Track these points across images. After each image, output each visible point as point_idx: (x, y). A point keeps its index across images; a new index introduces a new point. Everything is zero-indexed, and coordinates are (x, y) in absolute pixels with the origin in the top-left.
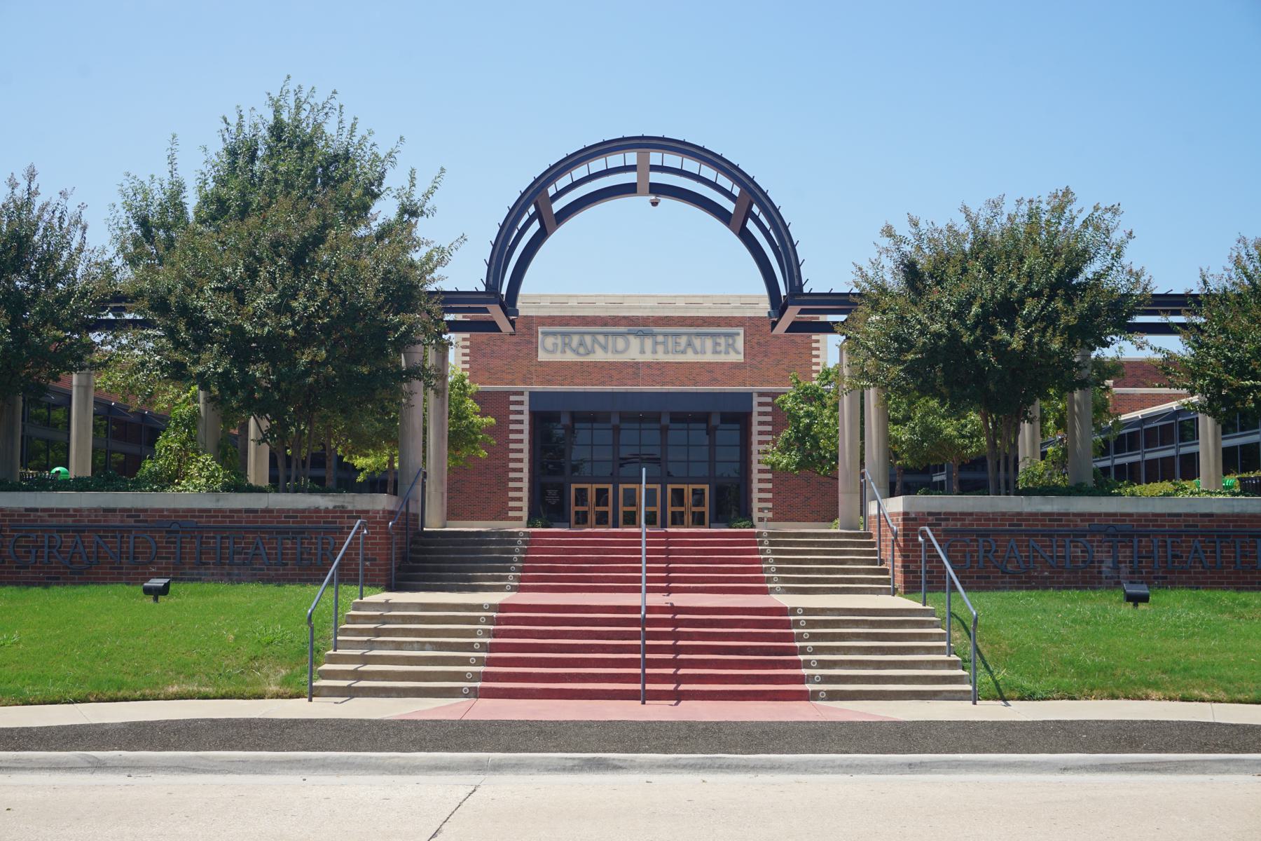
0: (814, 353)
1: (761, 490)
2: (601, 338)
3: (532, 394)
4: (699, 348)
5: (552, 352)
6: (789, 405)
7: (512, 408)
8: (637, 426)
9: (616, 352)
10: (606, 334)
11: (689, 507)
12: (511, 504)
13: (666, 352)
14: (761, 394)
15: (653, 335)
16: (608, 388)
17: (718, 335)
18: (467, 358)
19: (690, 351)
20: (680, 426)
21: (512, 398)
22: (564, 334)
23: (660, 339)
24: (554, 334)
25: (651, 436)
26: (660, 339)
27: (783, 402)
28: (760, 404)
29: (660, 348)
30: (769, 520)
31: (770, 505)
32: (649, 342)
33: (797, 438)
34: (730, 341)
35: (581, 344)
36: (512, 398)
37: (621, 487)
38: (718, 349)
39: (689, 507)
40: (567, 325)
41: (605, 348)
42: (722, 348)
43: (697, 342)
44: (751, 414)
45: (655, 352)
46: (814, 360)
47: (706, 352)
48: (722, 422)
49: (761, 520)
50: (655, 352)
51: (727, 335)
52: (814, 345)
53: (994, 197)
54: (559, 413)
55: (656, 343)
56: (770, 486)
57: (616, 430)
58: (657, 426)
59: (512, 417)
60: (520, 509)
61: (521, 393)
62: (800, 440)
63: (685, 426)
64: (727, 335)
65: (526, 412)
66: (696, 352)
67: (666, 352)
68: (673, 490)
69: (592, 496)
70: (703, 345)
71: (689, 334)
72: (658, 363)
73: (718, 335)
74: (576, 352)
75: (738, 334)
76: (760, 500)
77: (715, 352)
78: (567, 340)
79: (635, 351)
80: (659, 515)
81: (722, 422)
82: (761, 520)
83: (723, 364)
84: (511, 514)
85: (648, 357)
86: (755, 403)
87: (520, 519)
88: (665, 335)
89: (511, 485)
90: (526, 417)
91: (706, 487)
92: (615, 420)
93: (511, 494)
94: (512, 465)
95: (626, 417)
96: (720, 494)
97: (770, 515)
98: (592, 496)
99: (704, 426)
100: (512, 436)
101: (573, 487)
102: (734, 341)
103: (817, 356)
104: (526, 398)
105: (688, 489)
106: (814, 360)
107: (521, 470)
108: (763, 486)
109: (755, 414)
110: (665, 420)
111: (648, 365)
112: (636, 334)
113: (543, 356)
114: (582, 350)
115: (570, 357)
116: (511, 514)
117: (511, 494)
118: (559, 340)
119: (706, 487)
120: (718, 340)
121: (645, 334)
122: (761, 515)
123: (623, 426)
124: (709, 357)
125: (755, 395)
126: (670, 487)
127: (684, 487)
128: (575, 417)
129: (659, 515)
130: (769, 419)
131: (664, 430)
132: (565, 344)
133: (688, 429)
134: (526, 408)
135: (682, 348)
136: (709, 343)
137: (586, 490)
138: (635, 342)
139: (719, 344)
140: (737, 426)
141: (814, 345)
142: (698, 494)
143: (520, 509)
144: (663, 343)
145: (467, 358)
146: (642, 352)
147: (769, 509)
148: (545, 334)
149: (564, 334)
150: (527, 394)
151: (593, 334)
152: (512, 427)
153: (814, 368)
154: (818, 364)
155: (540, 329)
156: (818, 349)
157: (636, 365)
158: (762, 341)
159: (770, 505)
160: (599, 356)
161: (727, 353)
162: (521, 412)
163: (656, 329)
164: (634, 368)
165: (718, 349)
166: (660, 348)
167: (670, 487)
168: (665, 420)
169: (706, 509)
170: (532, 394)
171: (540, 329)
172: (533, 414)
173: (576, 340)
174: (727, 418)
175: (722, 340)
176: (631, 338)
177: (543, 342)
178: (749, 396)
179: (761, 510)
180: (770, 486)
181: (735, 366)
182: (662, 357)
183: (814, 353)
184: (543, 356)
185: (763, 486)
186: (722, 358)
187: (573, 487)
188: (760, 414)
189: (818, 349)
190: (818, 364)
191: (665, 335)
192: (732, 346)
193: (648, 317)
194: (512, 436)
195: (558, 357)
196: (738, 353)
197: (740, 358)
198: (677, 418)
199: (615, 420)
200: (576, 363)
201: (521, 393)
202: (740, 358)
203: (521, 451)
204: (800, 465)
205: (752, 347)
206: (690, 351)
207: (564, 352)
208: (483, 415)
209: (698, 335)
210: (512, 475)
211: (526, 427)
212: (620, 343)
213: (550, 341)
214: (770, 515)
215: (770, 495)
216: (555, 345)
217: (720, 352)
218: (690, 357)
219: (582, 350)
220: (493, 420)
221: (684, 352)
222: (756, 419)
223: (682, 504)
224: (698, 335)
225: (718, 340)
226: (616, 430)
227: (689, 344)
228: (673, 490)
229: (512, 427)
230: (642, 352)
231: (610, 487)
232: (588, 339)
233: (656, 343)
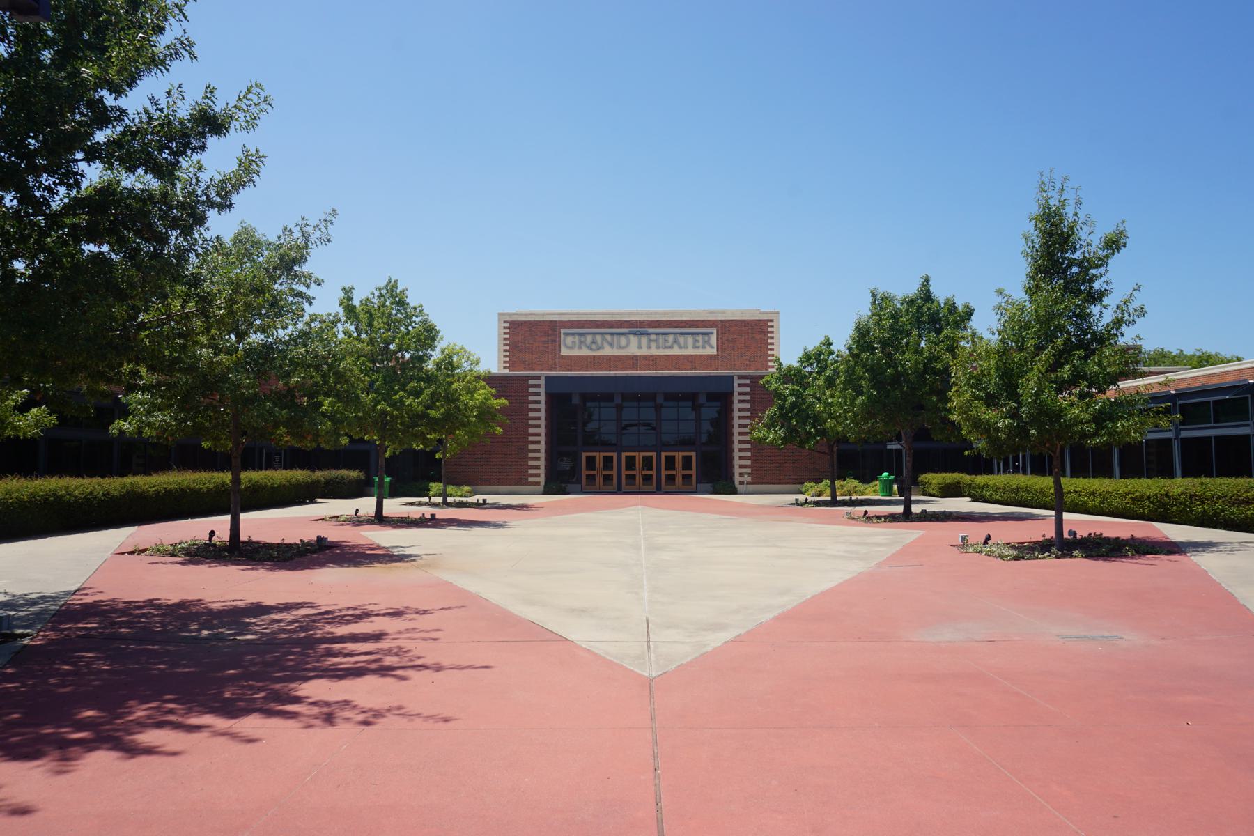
1: (741, 458)
2: (608, 338)
3: (548, 379)
6: (774, 385)
8: (636, 404)
9: (620, 347)
10: (612, 334)
11: (679, 471)
12: (531, 471)
13: (658, 347)
14: (741, 377)
15: (648, 334)
17: (698, 334)
19: (676, 346)
20: (671, 404)
21: (531, 382)
22: (581, 335)
23: (653, 337)
24: (573, 334)
25: (648, 414)
26: (653, 337)
27: (768, 382)
28: (740, 385)
29: (653, 345)
30: (749, 483)
31: (749, 471)
32: (644, 340)
33: (781, 414)
35: (594, 342)
36: (531, 382)
37: (624, 454)
39: (679, 471)
41: (611, 345)
43: (681, 339)
44: (732, 393)
45: (649, 347)
47: (688, 347)
48: (666, 399)
50: (649, 347)
51: (703, 334)
57: (619, 408)
61: (538, 378)
64: (703, 334)
65: (543, 393)
66: (680, 347)
67: (658, 347)
70: (686, 342)
73: (698, 334)
76: (741, 466)
77: (695, 347)
79: (634, 346)
80: (655, 478)
81: (666, 399)
84: (530, 479)
85: (644, 351)
86: (736, 384)
87: (538, 484)
88: (657, 334)
90: (542, 398)
92: (618, 400)
93: (531, 463)
94: (531, 439)
96: (704, 459)
97: (749, 479)
98: (599, 462)
99: (690, 404)
100: (531, 414)
101: (584, 455)
104: (542, 382)
107: (538, 443)
108: (743, 454)
109: (736, 394)
111: (645, 357)
112: (635, 334)
113: (564, 351)
115: (585, 352)
116: (530, 479)
117: (531, 463)
118: (577, 339)
119: (694, 454)
121: (642, 334)
122: (742, 479)
123: (625, 404)
124: (690, 351)
126: (663, 454)
127: (676, 454)
128: (585, 397)
129: (655, 478)
130: (748, 398)
131: (658, 408)
132: (581, 342)
134: (542, 390)
136: (690, 340)
140: (718, 404)
142: (687, 462)
143: (538, 475)
144: (656, 341)
146: (640, 347)
147: (748, 474)
148: (566, 334)
149: (581, 335)
150: (543, 379)
151: (602, 334)
152: (531, 406)
155: (562, 331)
157: (635, 358)
159: (749, 471)
160: (607, 351)
162: (741, 410)
163: (650, 330)
164: (634, 360)
166: (653, 345)
167: (663, 454)
168: (660, 400)
169: (693, 472)
171: (562, 331)
173: (589, 338)
174: (712, 397)
175: (700, 338)
176: (632, 337)
178: (731, 378)
181: (710, 357)
182: (654, 351)
184: (564, 351)
185: (743, 454)
186: (700, 352)
187: (584, 455)
191: (657, 334)
192: (708, 342)
194: (531, 414)
195: (576, 352)
197: (714, 351)
198: (670, 397)
199: (618, 400)
200: (589, 356)
201: (538, 378)
202: (714, 351)
203: (538, 426)
204: (784, 440)
206: (676, 346)
207: (580, 348)
208: (497, 397)
209: (682, 334)
210: (531, 447)
211: (542, 406)
212: (623, 341)
213: (569, 340)
214: (749, 479)
215: (749, 462)
218: (676, 351)
219: (594, 347)
220: (506, 402)
221: (671, 347)
222: (736, 398)
224: (682, 334)
226: (619, 408)
227: (675, 341)
229: (531, 406)
230: (640, 347)
231: (615, 455)
232: (598, 338)
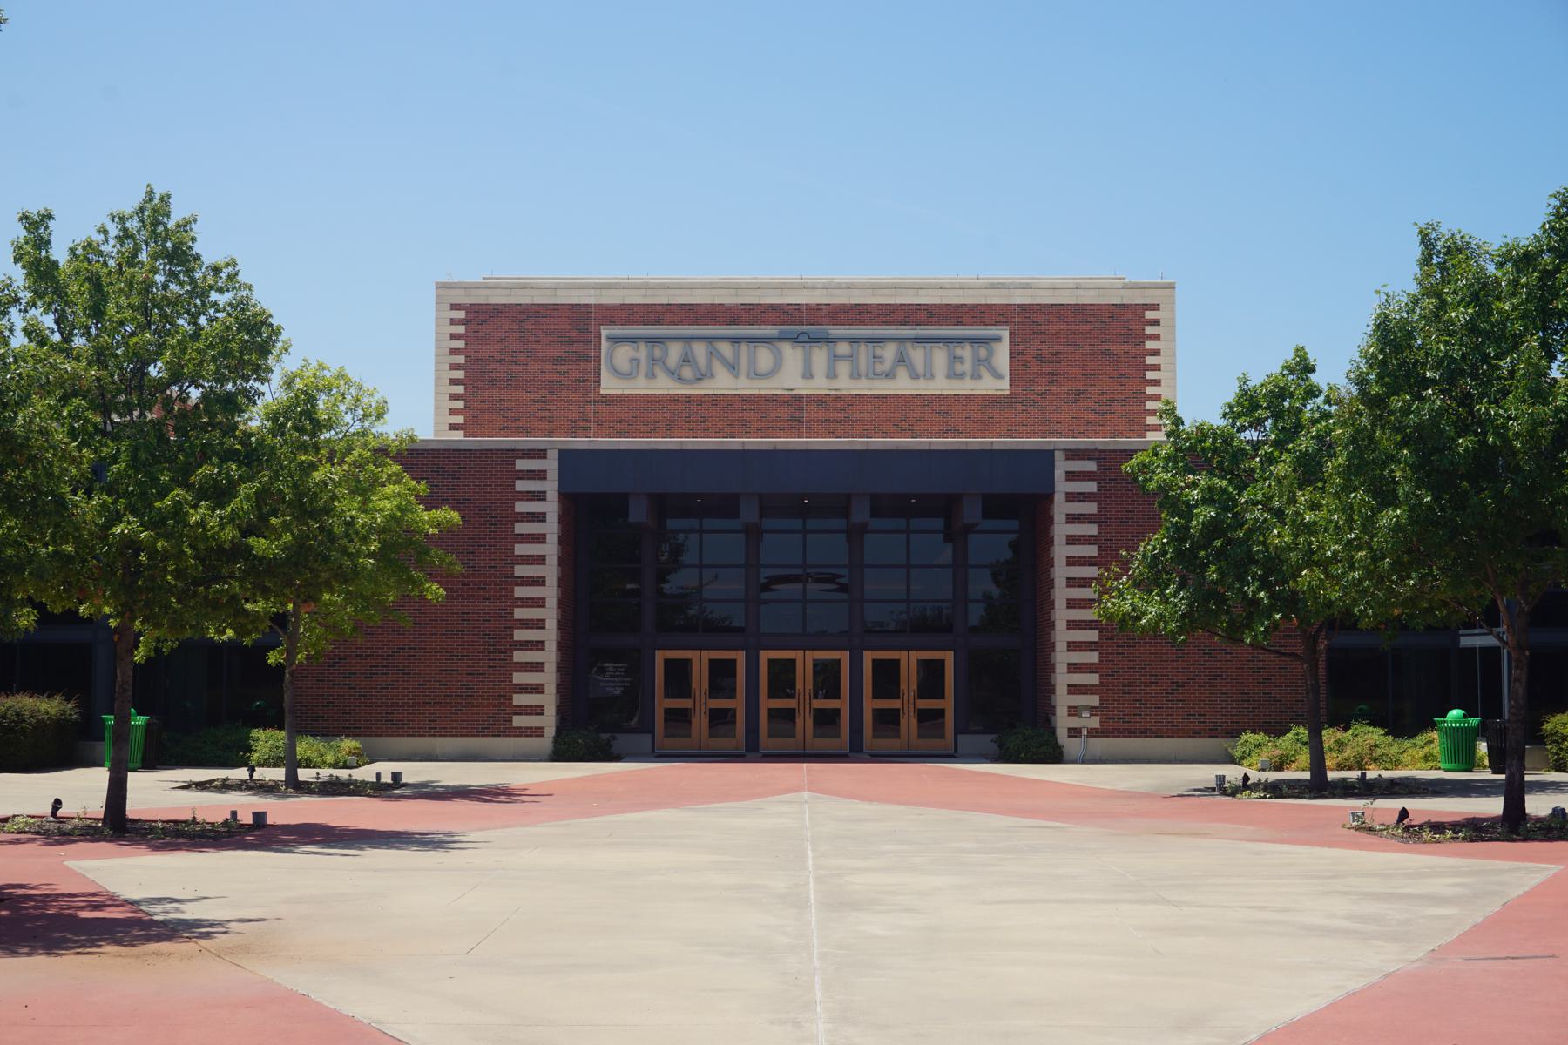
0: (1150, 375)
2: (725, 349)
3: (564, 455)
4: (920, 368)
5: (629, 376)
6: (1162, 476)
7: (521, 485)
8: (797, 524)
9: (756, 375)
10: (735, 340)
11: (908, 701)
14: (1073, 454)
15: (829, 340)
16: (878, 442)
17: (960, 340)
18: (460, 389)
19: (902, 373)
21: (521, 465)
22: (652, 341)
23: (843, 348)
24: (632, 340)
26: (843, 348)
27: (1144, 467)
29: (843, 368)
30: (1093, 733)
31: (1094, 700)
32: (820, 356)
33: (1180, 555)
34: (983, 353)
35: (687, 359)
36: (521, 465)
37: (765, 656)
38: (959, 368)
39: (908, 701)
40: (658, 322)
41: (733, 368)
42: (967, 367)
43: (917, 355)
44: (1049, 497)
46: (1150, 390)
47: (934, 375)
49: (1074, 733)
50: (832, 375)
51: (974, 341)
52: (1150, 360)
53: (34, 210)
54: (624, 497)
55: (835, 357)
56: (1094, 657)
57: (754, 534)
58: (839, 523)
59: (521, 507)
60: (538, 710)
61: (541, 454)
62: (1187, 558)
63: (901, 523)
64: (974, 341)
66: (915, 376)
68: (772, 662)
69: (804, 678)
70: (928, 362)
71: (901, 340)
72: (839, 397)
73: (960, 340)
74: (676, 375)
75: (998, 339)
77: (953, 375)
78: (658, 353)
79: (793, 372)
81: (987, 514)
82: (1074, 733)
83: (969, 398)
84: (518, 721)
85: (819, 386)
86: (1059, 474)
87: (538, 732)
88: (853, 341)
89: (519, 656)
90: (551, 507)
91: (948, 657)
95: (770, 506)
97: (1095, 722)
98: (804, 678)
100: (520, 549)
101: (661, 656)
102: (991, 354)
103: (1156, 383)
104: (551, 465)
105: (805, 660)
106: (1150, 390)
109: (1059, 498)
110: (860, 513)
111: (820, 401)
112: (795, 340)
113: (610, 385)
114: (687, 372)
115: (664, 386)
116: (518, 721)
118: (643, 352)
119: (948, 657)
120: (959, 352)
121: (815, 340)
122: (1074, 722)
123: (768, 523)
124: (940, 386)
125: (1059, 456)
126: (868, 656)
127: (901, 655)
128: (663, 505)
131: (856, 534)
132: (654, 360)
133: (701, 532)
134: (551, 487)
135: (887, 366)
136: (940, 356)
137: (686, 663)
138: (792, 355)
139: (961, 359)
141: (1150, 360)
142: (931, 677)
144: (851, 357)
145: (460, 389)
146: (808, 374)
147: (1093, 710)
148: (615, 340)
149: (652, 341)
150: (553, 456)
152: (520, 528)
153: (1150, 405)
154: (1157, 398)
155: (605, 331)
156: (1157, 368)
157: (795, 402)
158: (1046, 353)
159: (1094, 700)
160: (723, 383)
161: (976, 376)
163: (836, 331)
164: (792, 409)
165: (959, 368)
166: (843, 368)
169: (948, 704)
170: (564, 455)
171: (605, 331)
172: (565, 497)
173: (675, 351)
174: (996, 506)
175: (966, 352)
176: (787, 349)
177: (610, 355)
178: (1047, 457)
179: (1074, 711)
180: (1094, 657)
181: (992, 402)
182: (845, 385)
183: (1150, 375)
184: (610, 385)
186: (965, 387)
187: (661, 656)
188: (1072, 497)
189: (1157, 368)
190: (1157, 398)
191: (853, 341)
193: (819, 307)
195: (639, 386)
196: (999, 376)
197: (1002, 386)
198: (885, 506)
199: (749, 512)
201: (541, 454)
202: (1002, 386)
205: (1026, 365)
206: (902, 373)
207: (651, 375)
209: (918, 340)
212: (764, 357)
213: (623, 354)
214: (1095, 722)
215: (1094, 679)
216: (635, 361)
217: (961, 376)
218: (903, 385)
219: (687, 372)
220: (455, 516)
221: (890, 375)
223: (685, 693)
224: (918, 340)
225: (959, 352)
226: (754, 534)
227: (901, 359)
228: (772, 662)
231: (740, 657)
232: (700, 350)
233: (835, 357)
